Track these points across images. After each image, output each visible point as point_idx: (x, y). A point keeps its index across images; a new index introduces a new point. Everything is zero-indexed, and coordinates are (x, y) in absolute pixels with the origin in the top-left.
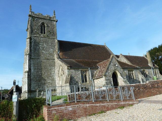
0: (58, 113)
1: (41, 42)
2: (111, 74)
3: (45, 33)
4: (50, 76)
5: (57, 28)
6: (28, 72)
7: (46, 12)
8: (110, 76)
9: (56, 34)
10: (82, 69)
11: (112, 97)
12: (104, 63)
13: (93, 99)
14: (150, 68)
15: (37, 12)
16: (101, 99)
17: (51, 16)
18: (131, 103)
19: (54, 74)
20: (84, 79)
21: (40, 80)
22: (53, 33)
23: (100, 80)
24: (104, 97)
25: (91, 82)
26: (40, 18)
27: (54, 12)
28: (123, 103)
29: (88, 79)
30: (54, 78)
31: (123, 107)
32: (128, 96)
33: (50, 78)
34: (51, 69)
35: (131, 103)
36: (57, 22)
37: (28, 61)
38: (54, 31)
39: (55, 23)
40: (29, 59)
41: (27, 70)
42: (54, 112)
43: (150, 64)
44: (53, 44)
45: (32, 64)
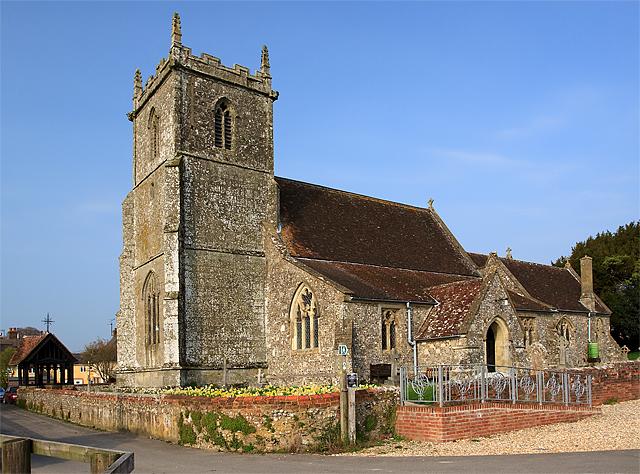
0: (460, 421)
1: (218, 184)
2: (484, 329)
3: (228, 147)
4: (247, 318)
5: (275, 128)
6: (178, 298)
7: (236, 55)
8: (481, 336)
9: (271, 155)
10: (384, 306)
11: (548, 395)
12: (456, 290)
13: (514, 398)
14: (584, 312)
15: (201, 44)
16: (463, 399)
17: (254, 74)
18: (586, 412)
19: (261, 311)
20: (387, 336)
21: (215, 328)
22: (263, 153)
23: (443, 345)
24: (506, 393)
25: (409, 348)
26: (213, 78)
27: (265, 57)
28: (570, 411)
29: (399, 339)
30: (261, 323)
31: (571, 419)
32: (579, 395)
33: (248, 322)
34: (250, 292)
35: (586, 412)
36: (274, 99)
37: (177, 255)
38: (261, 139)
39: (266, 103)
40: (179, 250)
41: (176, 288)
42: (453, 419)
43: (588, 301)
44: (259, 192)
45: (186, 267)
